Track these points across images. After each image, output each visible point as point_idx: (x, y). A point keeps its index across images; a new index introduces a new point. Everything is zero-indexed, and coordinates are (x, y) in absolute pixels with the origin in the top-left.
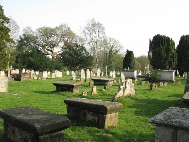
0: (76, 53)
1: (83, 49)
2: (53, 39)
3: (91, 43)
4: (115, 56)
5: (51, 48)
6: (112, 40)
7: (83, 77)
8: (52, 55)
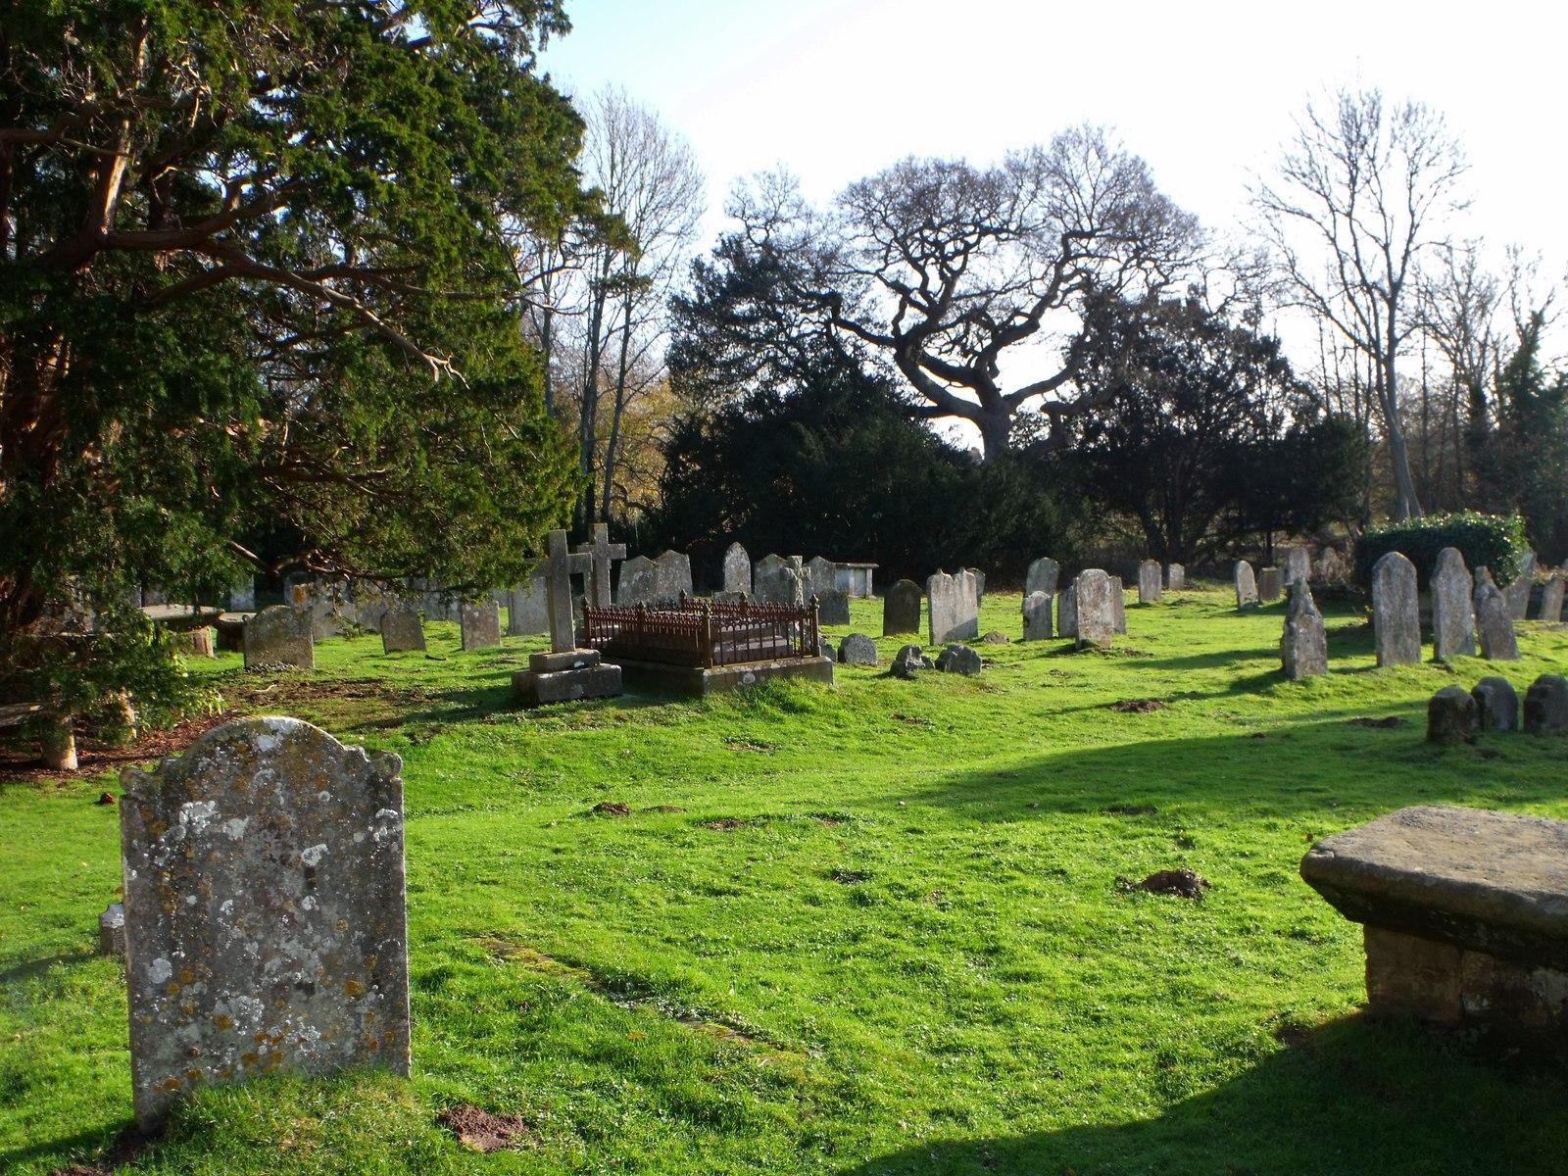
1: (1264, 353)
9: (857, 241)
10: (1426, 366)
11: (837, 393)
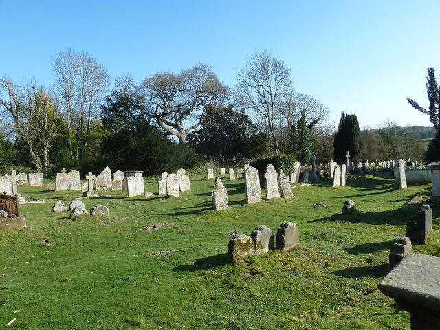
0: (230, 128)
1: (244, 118)
2: (178, 99)
3: (260, 108)
4: (312, 132)
5: (177, 120)
6: (304, 99)
7: (254, 195)
8: (179, 135)
9: (146, 92)
10: (280, 122)
11: (142, 127)
